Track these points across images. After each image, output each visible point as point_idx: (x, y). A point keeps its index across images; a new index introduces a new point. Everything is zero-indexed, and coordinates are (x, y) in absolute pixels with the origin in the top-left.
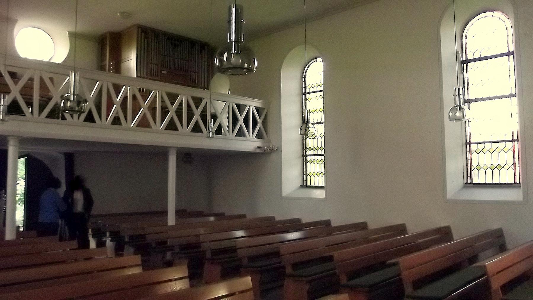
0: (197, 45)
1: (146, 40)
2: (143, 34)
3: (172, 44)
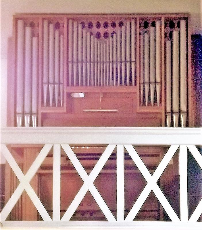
0: (158, 24)
1: (35, 40)
2: (28, 30)
3: (98, 35)
